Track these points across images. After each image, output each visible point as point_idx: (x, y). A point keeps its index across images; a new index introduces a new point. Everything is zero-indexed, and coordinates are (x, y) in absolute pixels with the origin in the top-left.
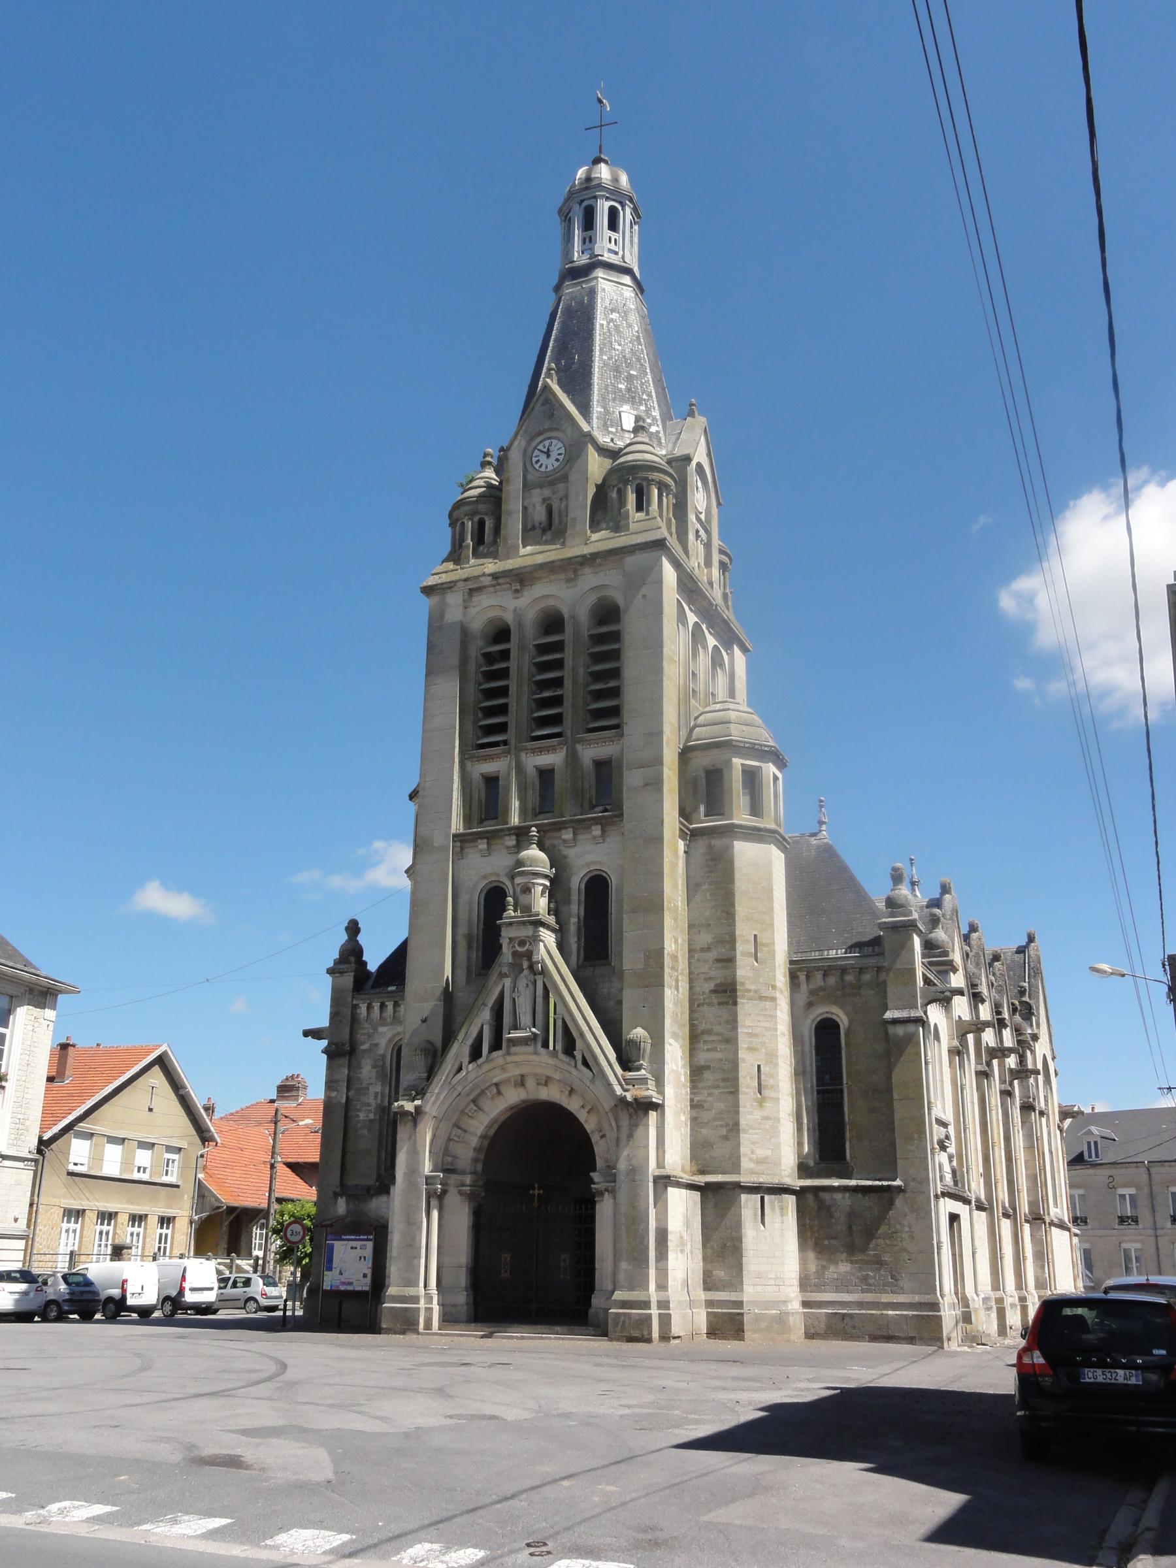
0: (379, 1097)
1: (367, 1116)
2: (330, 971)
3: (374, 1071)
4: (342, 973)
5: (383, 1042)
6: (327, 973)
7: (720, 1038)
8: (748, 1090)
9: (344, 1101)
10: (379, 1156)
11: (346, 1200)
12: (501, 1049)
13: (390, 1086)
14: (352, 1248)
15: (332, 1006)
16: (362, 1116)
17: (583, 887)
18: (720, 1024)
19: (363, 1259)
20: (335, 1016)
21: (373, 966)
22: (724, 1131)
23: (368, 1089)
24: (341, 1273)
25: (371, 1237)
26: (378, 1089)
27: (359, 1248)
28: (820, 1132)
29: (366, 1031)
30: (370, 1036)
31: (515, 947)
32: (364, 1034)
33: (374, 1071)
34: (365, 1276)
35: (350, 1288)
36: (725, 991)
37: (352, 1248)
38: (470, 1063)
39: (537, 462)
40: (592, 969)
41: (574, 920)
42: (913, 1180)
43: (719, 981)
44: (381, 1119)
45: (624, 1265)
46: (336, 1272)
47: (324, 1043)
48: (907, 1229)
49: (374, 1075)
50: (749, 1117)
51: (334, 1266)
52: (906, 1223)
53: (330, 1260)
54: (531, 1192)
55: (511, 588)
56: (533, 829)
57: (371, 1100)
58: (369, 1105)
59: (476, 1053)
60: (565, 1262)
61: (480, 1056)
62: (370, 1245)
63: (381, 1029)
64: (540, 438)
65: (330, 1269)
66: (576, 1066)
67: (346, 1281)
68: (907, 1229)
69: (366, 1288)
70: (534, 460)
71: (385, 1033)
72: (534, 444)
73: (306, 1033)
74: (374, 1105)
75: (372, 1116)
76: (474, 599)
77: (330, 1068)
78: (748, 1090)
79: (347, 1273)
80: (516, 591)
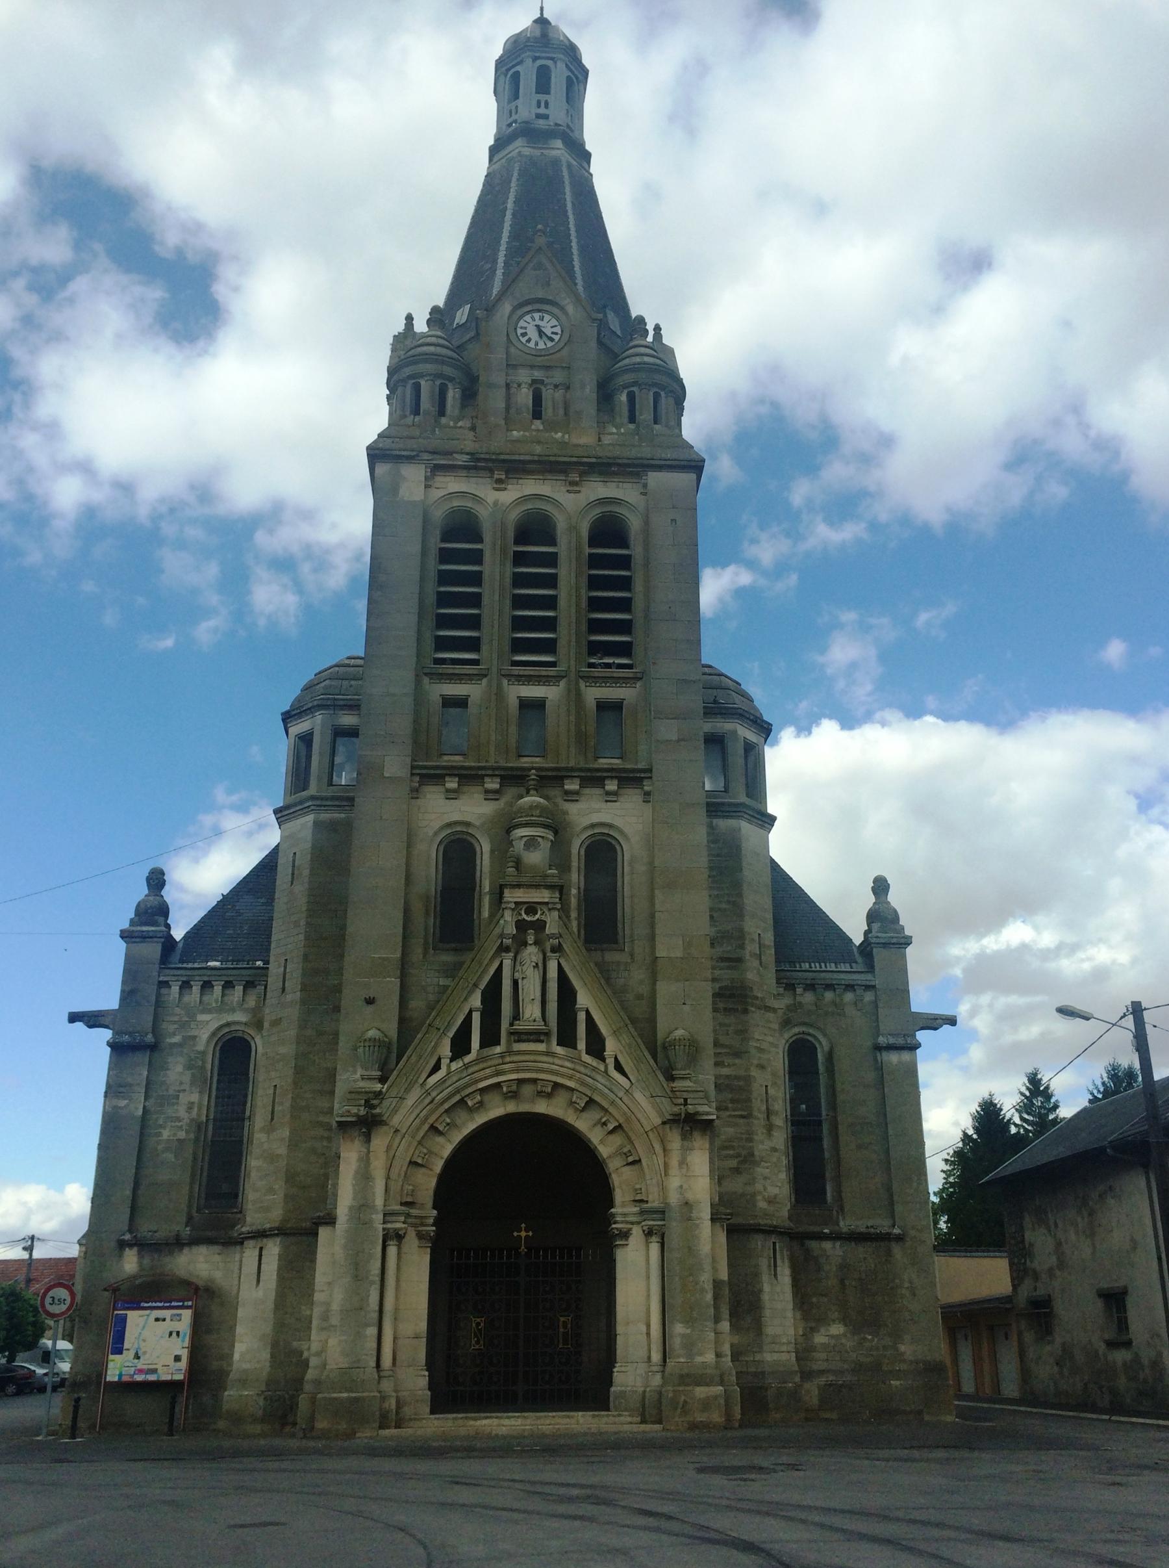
0: (196, 1109)
1: (175, 1135)
2: (124, 935)
3: (188, 1073)
4: (144, 937)
5: (204, 1035)
6: (122, 937)
7: (728, 1051)
8: (759, 1115)
9: (140, 1112)
10: (191, 1188)
11: (138, 1251)
12: (499, 1044)
13: (209, 1097)
14: (157, 1320)
15: (124, 982)
16: (166, 1134)
17: (583, 852)
18: (728, 1034)
19: (174, 1334)
20: (128, 995)
21: (178, 933)
22: (733, 1163)
23: (177, 1097)
24: (137, 1357)
25: (190, 1303)
26: (195, 1097)
27: (168, 1319)
28: (795, 1167)
29: (176, 1019)
30: (184, 1025)
31: (521, 915)
32: (175, 1022)
33: (188, 1073)
34: (177, 1359)
35: (152, 1378)
36: (732, 996)
37: (157, 1320)
38: (452, 1060)
39: (524, 335)
40: (599, 953)
41: (574, 891)
42: (913, 1228)
43: (723, 984)
44: (197, 1140)
45: (679, 1329)
46: (128, 1356)
47: (107, 1034)
48: (907, 1285)
49: (187, 1078)
50: (761, 1146)
51: (126, 1346)
52: (906, 1277)
53: (120, 1337)
54: (515, 1234)
55: (492, 477)
56: (533, 771)
57: (182, 1112)
58: (179, 1119)
59: (460, 1046)
60: (565, 1327)
61: (468, 1051)
62: (187, 1315)
63: (202, 1017)
64: (529, 308)
65: (119, 1351)
66: (606, 1072)
67: (146, 1367)
68: (907, 1285)
69: (179, 1377)
70: (520, 331)
71: (208, 1022)
72: (520, 312)
73: (74, 1018)
74: (186, 1121)
75: (182, 1135)
76: (438, 479)
77: (114, 1066)
78: (759, 1115)
79: (147, 1356)
80: (499, 481)
